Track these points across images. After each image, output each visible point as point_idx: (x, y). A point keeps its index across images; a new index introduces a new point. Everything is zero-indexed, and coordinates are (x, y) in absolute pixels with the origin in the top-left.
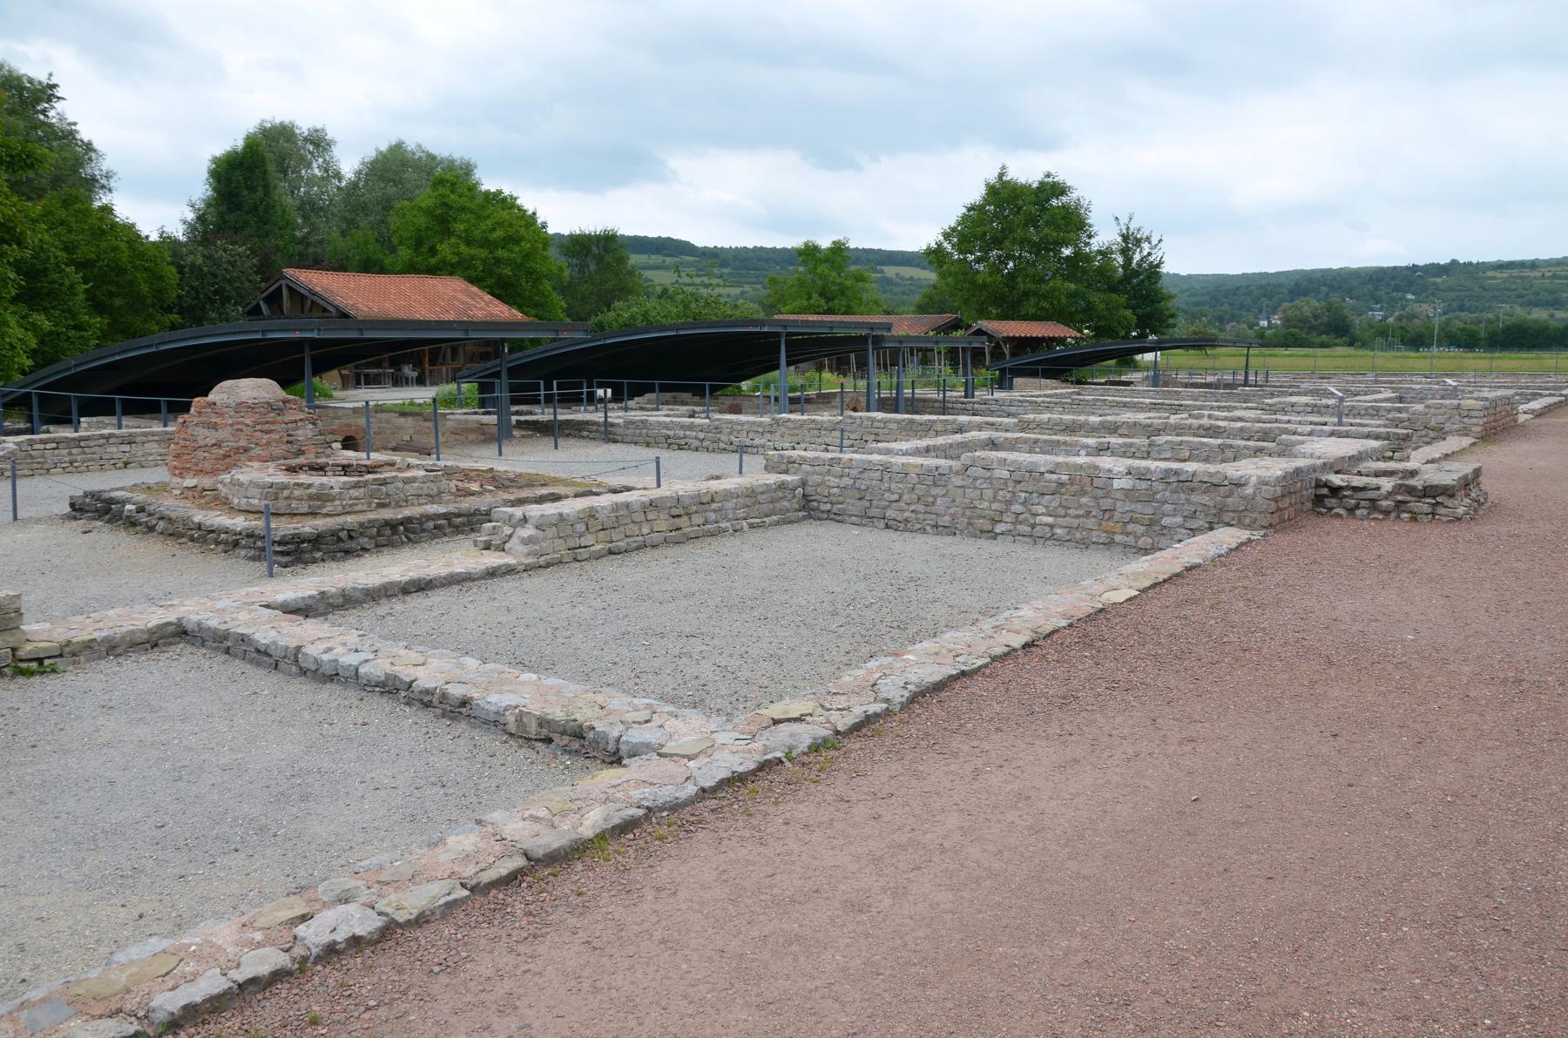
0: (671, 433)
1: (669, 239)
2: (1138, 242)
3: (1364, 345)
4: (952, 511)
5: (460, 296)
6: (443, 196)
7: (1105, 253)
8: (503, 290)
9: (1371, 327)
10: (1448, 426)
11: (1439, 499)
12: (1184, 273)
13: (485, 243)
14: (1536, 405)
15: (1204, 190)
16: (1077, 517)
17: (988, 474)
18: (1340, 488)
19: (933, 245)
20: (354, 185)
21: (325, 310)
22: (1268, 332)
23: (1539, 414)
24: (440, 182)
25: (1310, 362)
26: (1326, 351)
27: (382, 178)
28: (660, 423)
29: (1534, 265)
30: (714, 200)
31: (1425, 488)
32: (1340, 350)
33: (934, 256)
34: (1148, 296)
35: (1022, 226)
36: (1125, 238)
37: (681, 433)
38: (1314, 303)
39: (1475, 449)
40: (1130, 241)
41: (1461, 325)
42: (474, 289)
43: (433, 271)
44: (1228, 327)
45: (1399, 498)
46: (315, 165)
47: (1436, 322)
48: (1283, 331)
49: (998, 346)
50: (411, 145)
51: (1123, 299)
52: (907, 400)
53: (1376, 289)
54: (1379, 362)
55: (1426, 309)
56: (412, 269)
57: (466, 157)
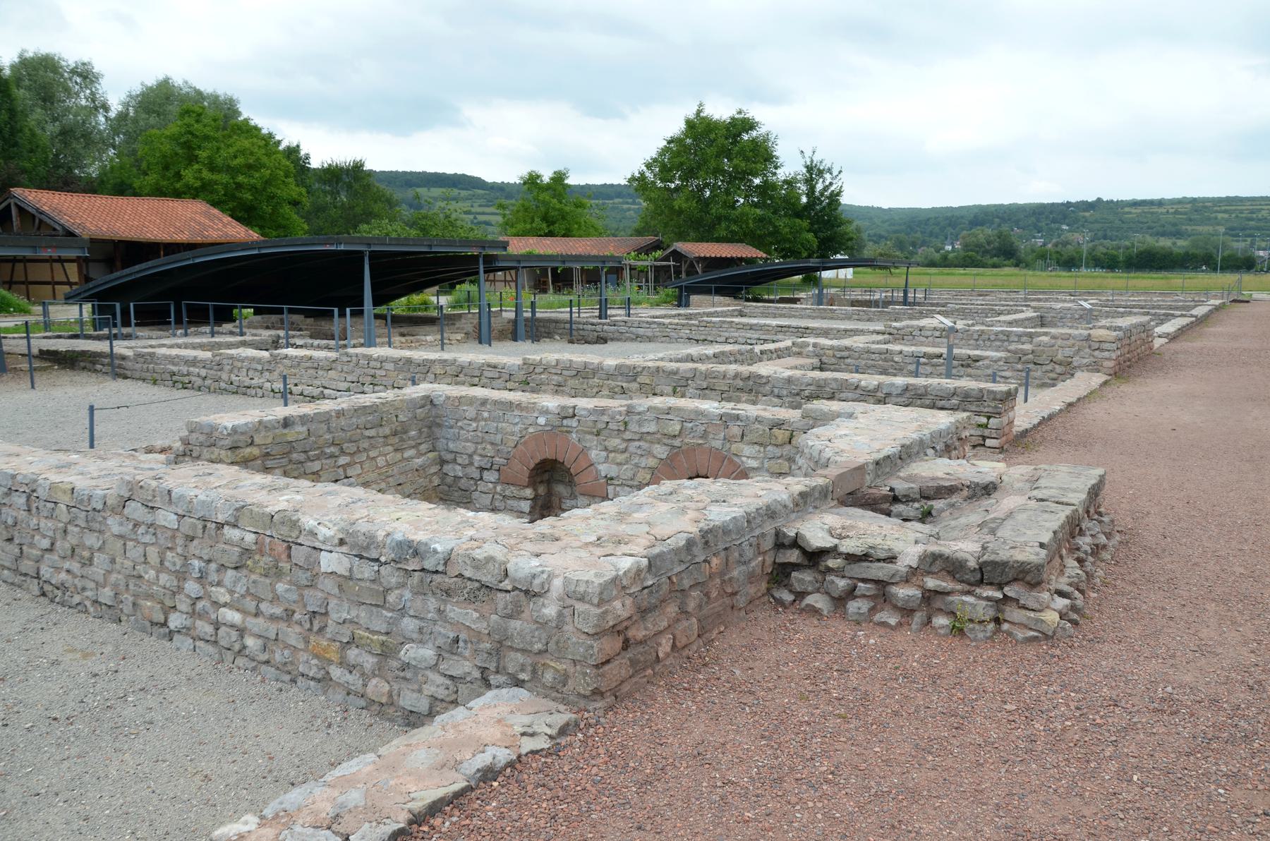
0: (175, 369)
1: (464, 175)
2: (820, 173)
3: (1028, 266)
4: (113, 577)
5: (197, 217)
6: (188, 125)
7: (789, 183)
8: (245, 214)
9: (1033, 251)
10: (1076, 361)
11: (1010, 591)
12: (885, 207)
13: (232, 171)
14: (1170, 327)
15: (882, 134)
16: (273, 618)
17: (149, 518)
18: (822, 553)
19: (637, 175)
20: (122, 116)
21: (55, 229)
22: (951, 255)
23: (1173, 338)
24: (187, 112)
25: (969, 280)
26: (995, 271)
27: (148, 111)
28: (166, 357)
29: (1160, 203)
30: (495, 145)
31: (982, 568)
32: (1007, 270)
33: (639, 184)
34: (829, 221)
35: (718, 157)
36: (810, 169)
37: (184, 369)
38: (989, 231)
39: (1107, 389)
40: (814, 172)
41: (1105, 251)
42: (216, 211)
43: (178, 195)
44: (920, 251)
45: (931, 583)
46: (82, 95)
47: (1085, 248)
48: (962, 254)
49: (692, 266)
50: (178, 80)
51: (805, 224)
52: (527, 320)
53: (1038, 220)
54: (1031, 280)
55: (1077, 237)
56: (159, 192)
57: (229, 93)
